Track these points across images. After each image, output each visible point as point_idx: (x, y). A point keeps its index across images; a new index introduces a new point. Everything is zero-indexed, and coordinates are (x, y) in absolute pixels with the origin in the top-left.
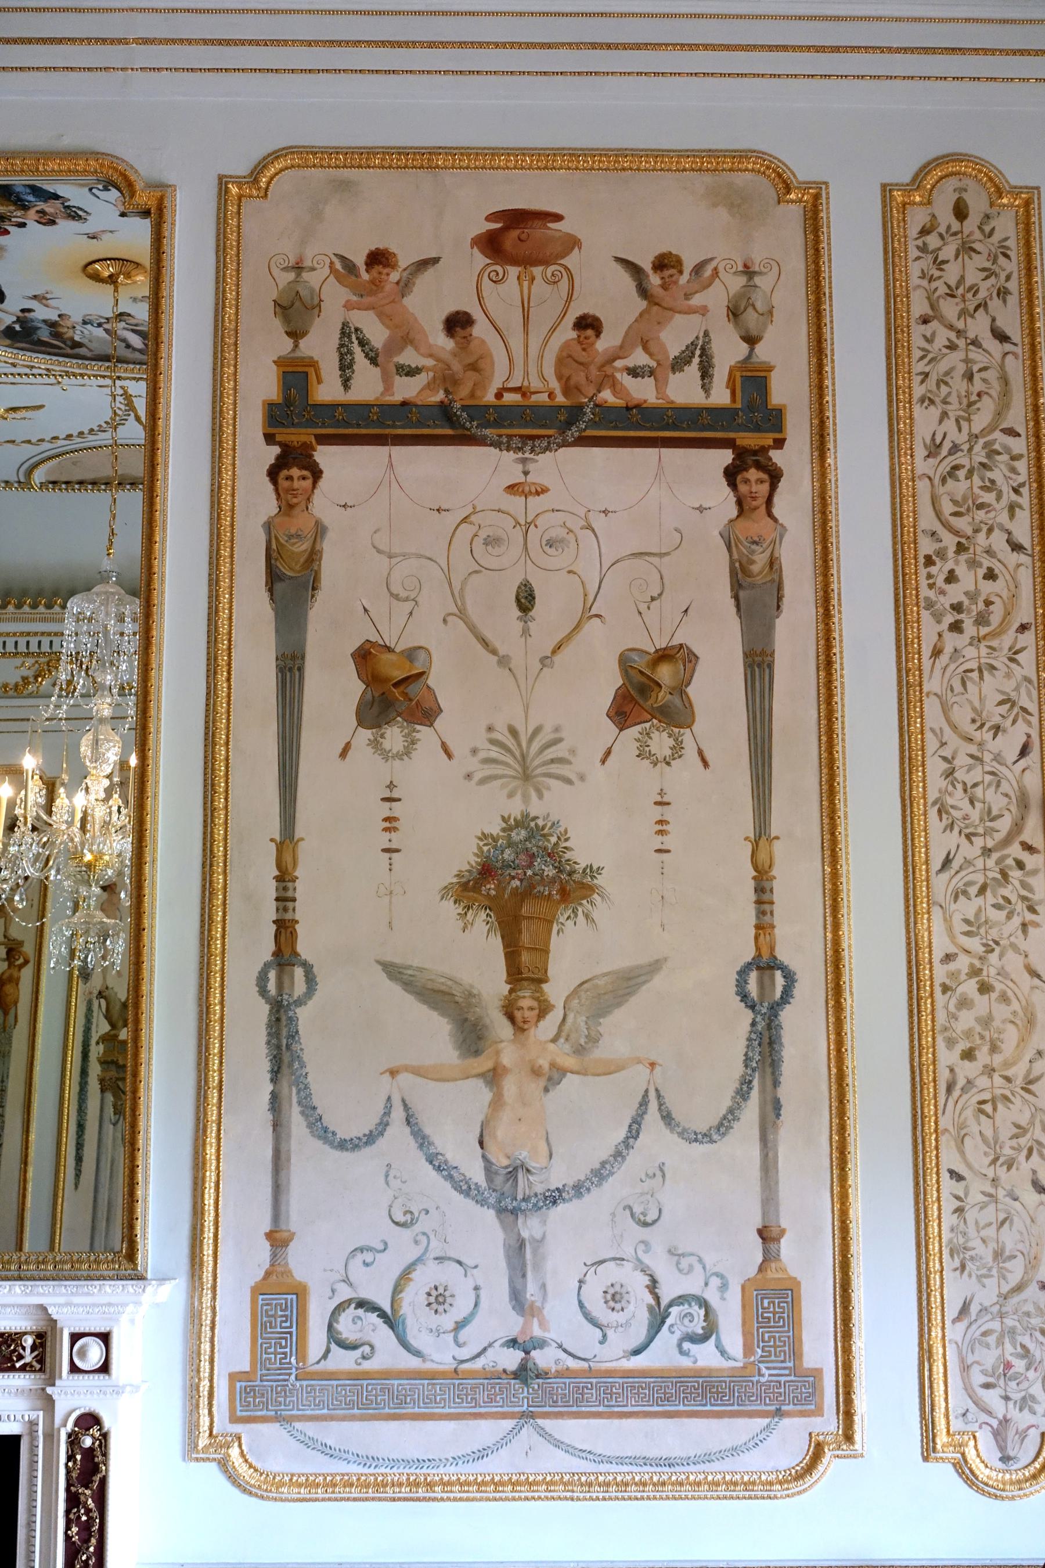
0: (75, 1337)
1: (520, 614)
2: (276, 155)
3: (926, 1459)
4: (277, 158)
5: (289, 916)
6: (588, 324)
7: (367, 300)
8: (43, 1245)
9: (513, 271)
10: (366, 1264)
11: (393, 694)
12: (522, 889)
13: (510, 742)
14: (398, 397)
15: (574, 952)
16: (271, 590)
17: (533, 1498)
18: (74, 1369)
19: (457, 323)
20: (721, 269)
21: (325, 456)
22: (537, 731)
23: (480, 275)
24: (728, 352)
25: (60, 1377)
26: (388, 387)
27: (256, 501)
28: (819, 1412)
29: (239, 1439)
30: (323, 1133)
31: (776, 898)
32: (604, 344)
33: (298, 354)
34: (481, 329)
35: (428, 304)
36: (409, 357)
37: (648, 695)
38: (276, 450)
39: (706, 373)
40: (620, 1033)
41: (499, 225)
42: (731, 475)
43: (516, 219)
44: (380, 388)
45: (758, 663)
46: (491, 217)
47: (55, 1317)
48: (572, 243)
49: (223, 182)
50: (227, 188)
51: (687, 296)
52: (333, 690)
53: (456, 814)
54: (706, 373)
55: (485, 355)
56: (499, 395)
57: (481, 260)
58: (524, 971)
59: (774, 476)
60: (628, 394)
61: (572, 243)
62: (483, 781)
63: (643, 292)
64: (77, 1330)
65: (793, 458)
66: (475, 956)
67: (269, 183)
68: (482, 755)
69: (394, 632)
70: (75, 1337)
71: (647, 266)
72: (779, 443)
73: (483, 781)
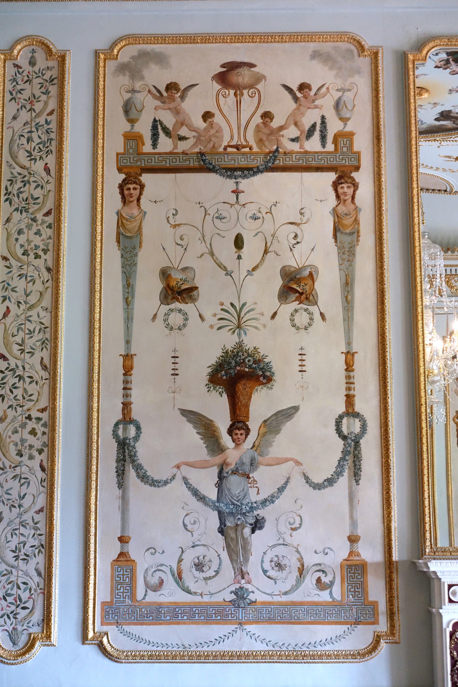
0: (450, 586)
1: (236, 250)
2: (120, 39)
3: (83, 643)
4: (122, 40)
5: (352, 392)
6: (267, 116)
7: (167, 106)
8: (447, 545)
9: (232, 92)
10: (152, 554)
11: (177, 292)
12: (238, 375)
13: (232, 310)
14: (179, 150)
15: (261, 404)
16: (118, 242)
17: (7, 663)
18: (451, 601)
19: (207, 116)
20: (330, 88)
21: (145, 178)
22: (244, 304)
23: (218, 95)
24: (334, 126)
25: (445, 605)
26: (176, 147)
27: (112, 201)
28: (375, 622)
29: (107, 634)
30: (143, 477)
31: (355, 381)
32: (275, 124)
33: (133, 131)
34: (218, 119)
35: (192, 108)
36: (183, 132)
37: (296, 286)
38: (123, 176)
39: (323, 138)
40: (281, 445)
41: (225, 69)
42: (335, 185)
43: (232, 67)
44: (172, 147)
45: (348, 284)
46: (223, 66)
47: (440, 577)
48: (260, 78)
49: (97, 53)
50: (99, 55)
51: (314, 101)
52: (149, 287)
53: (207, 347)
54: (323, 138)
55: (220, 130)
56: (225, 149)
57: (217, 87)
58: (238, 425)
59: (355, 186)
60: (286, 148)
61: (260, 78)
62: (219, 328)
63: (296, 99)
64: (451, 583)
65: (364, 177)
66: (218, 408)
67: (118, 52)
68: (219, 317)
69: (176, 258)
70: (450, 586)
71: (295, 88)
72: (357, 168)
73: (219, 328)
